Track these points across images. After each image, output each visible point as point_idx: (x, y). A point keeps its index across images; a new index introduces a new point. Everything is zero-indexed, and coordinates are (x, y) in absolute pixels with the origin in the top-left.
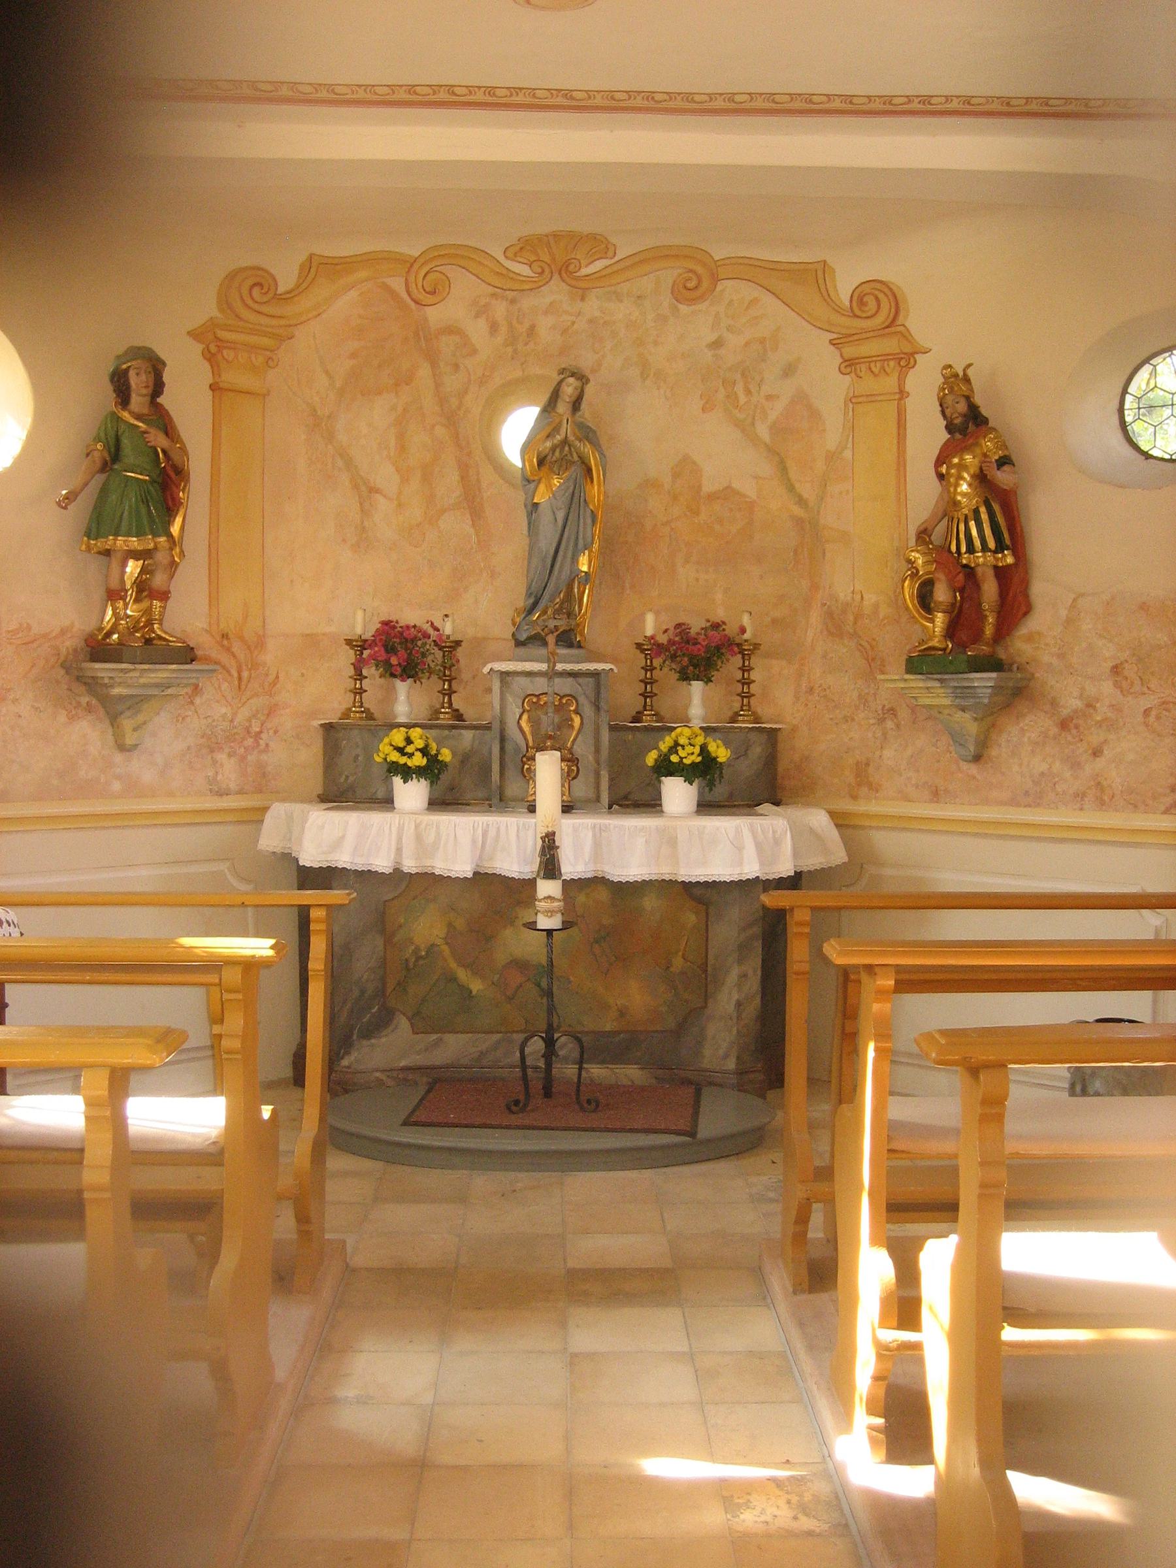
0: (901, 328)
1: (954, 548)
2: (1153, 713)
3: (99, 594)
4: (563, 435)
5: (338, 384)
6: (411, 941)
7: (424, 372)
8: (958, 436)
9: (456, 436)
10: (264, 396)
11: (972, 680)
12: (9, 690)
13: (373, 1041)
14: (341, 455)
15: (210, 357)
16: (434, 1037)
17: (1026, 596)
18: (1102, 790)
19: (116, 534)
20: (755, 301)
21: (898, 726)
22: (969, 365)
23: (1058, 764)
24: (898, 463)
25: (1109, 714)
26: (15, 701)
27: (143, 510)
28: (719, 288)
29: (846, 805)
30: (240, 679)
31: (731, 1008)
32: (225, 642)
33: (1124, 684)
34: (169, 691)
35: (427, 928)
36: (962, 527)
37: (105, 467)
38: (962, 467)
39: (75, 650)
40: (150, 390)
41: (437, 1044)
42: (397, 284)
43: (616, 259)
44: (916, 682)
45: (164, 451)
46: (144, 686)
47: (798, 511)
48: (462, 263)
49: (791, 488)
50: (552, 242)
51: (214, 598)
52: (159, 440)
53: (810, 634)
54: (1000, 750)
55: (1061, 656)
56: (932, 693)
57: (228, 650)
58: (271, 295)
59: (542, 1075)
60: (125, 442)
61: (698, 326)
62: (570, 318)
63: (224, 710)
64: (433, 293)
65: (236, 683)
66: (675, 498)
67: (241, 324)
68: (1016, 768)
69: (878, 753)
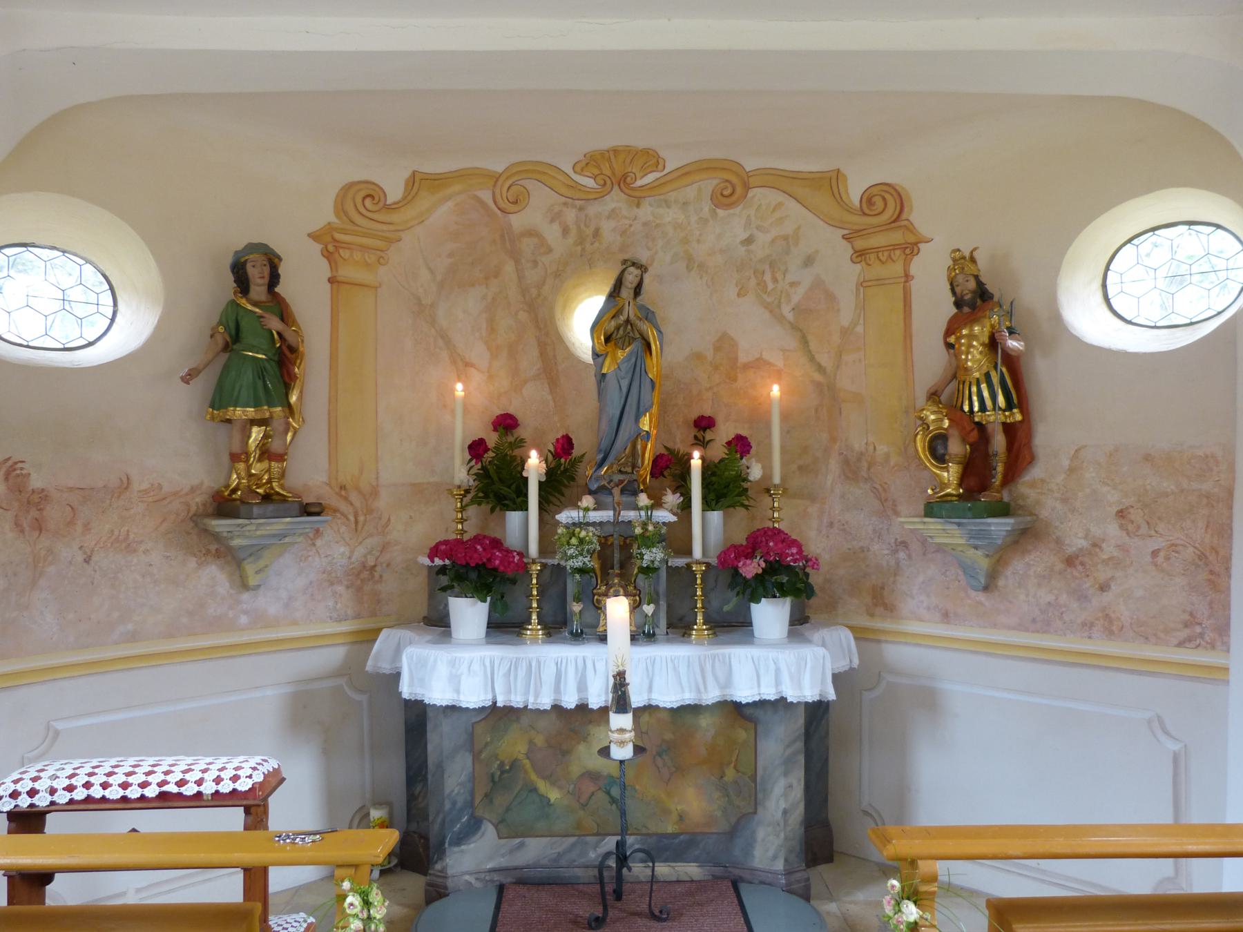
0: (906, 223)
1: (966, 408)
2: (1162, 554)
5: (439, 278)
6: (496, 757)
7: (509, 268)
11: (989, 525)
12: (141, 542)
13: (463, 847)
14: (442, 337)
15: (328, 255)
16: (518, 841)
17: (1030, 448)
18: (1111, 622)
19: (236, 406)
20: (780, 205)
21: (910, 556)
22: (975, 249)
23: (1065, 596)
24: (905, 337)
25: (1115, 554)
26: (146, 552)
27: (260, 383)
28: (750, 194)
30: (356, 522)
31: (779, 815)
32: (343, 493)
33: (1130, 527)
34: (287, 540)
35: (514, 745)
36: (974, 389)
37: (226, 348)
38: (971, 337)
39: (204, 505)
40: (266, 280)
42: (486, 196)
45: (279, 333)
46: (263, 536)
47: (818, 377)
48: (538, 177)
49: (812, 359)
50: (612, 157)
51: (333, 457)
52: (275, 324)
53: (830, 478)
54: (1007, 580)
55: (1065, 501)
57: (346, 499)
58: (381, 204)
60: (243, 324)
61: (732, 227)
62: (627, 222)
63: (342, 549)
64: (516, 202)
65: (353, 526)
68: (1022, 597)
69: (892, 579)
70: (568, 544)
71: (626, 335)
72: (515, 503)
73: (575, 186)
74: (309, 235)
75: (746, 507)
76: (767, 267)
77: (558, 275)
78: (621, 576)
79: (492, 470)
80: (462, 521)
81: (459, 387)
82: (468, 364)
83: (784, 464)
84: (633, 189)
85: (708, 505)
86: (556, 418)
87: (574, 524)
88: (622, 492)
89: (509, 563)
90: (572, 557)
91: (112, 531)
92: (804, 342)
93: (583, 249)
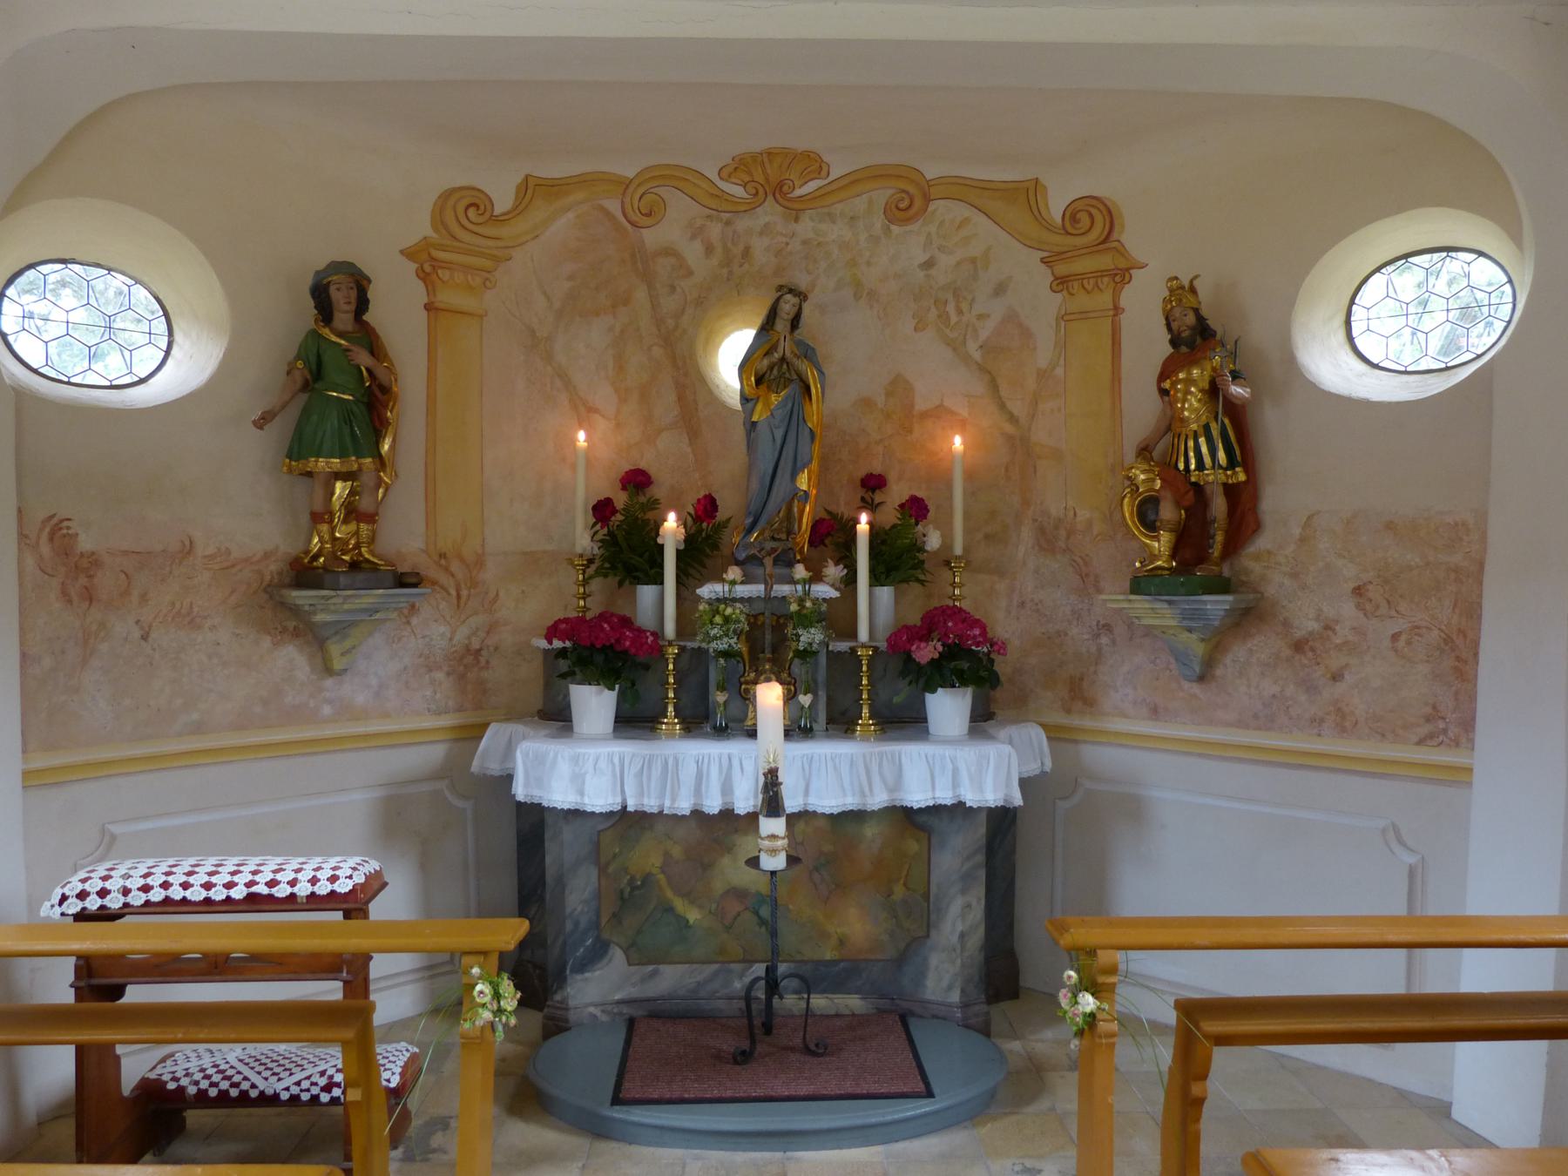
1: (1181, 466)
2: (1404, 637)
3: (305, 519)
6: (626, 870)
7: (641, 294)
8: (1184, 349)
10: (481, 317)
11: (1205, 602)
15: (423, 276)
16: (651, 968)
19: (318, 456)
20: (966, 221)
21: (1114, 642)
22: (1196, 277)
25: (1350, 638)
26: (213, 628)
27: (347, 431)
29: (1059, 718)
30: (459, 597)
31: (955, 939)
33: (1368, 607)
34: (378, 616)
35: (647, 857)
36: (1191, 443)
37: (306, 387)
38: (1189, 381)
40: (353, 307)
41: (654, 974)
42: (613, 206)
43: (830, 179)
44: (1141, 604)
47: (1009, 428)
49: (1002, 406)
52: (364, 359)
53: (1022, 549)
54: (1227, 667)
55: (1294, 575)
56: (1155, 612)
57: (447, 569)
58: (487, 215)
59: (763, 1007)
64: (649, 215)
67: (456, 244)
70: (711, 623)
71: (782, 375)
73: (721, 196)
74: (402, 252)
75: (922, 582)
76: (950, 297)
77: (700, 302)
79: (620, 536)
80: (585, 597)
82: (591, 410)
84: (790, 200)
85: (876, 579)
86: (697, 475)
87: (718, 600)
90: (715, 638)
91: (173, 604)
92: (994, 386)
93: (731, 273)
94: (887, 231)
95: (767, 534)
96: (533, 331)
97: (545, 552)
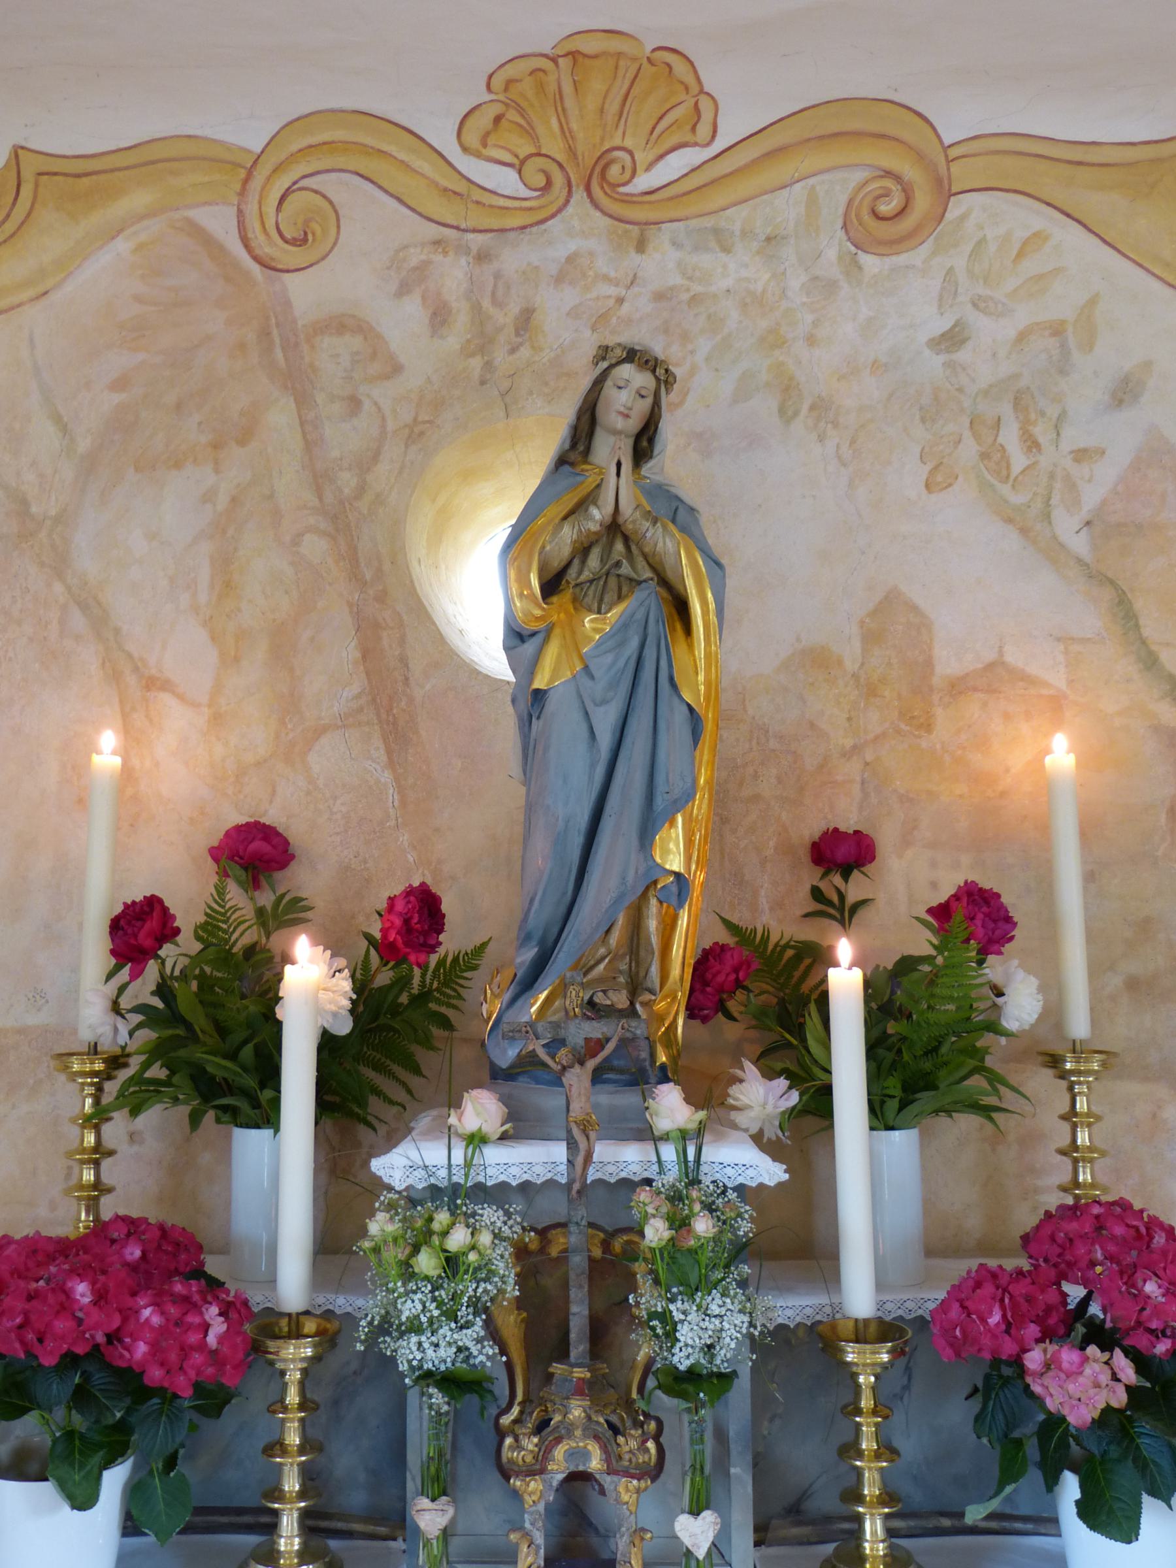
4: (609, 509)
5: (84, 445)
7: (281, 417)
9: (351, 558)
14: (84, 607)
20: (1037, 239)
28: (956, 208)
42: (219, 222)
61: (907, 300)
62: (612, 291)
64: (301, 241)
66: (871, 691)
70: (408, 1272)
71: (609, 571)
72: (256, 1105)
73: (465, 192)
75: (986, 1111)
76: (1006, 409)
77: (414, 434)
78: (591, 1389)
79: (187, 993)
80: (99, 1155)
81: (108, 740)
82: (154, 683)
83: (1096, 969)
84: (628, 199)
85: (881, 1115)
86: (404, 838)
87: (434, 1191)
88: (597, 1077)
89: (185, 1351)
90: (414, 1327)
92: (1125, 613)
93: (488, 366)
94: (852, 267)
95: (576, 996)
96: (24, 503)
97: (21, 1031)
